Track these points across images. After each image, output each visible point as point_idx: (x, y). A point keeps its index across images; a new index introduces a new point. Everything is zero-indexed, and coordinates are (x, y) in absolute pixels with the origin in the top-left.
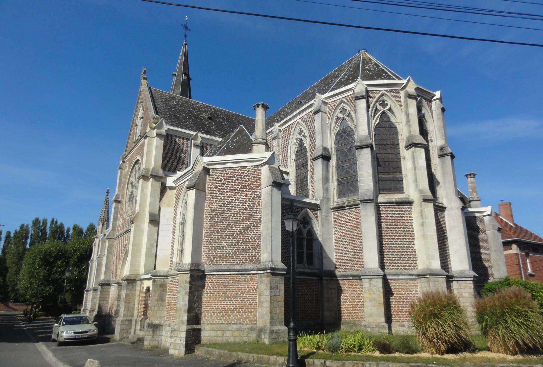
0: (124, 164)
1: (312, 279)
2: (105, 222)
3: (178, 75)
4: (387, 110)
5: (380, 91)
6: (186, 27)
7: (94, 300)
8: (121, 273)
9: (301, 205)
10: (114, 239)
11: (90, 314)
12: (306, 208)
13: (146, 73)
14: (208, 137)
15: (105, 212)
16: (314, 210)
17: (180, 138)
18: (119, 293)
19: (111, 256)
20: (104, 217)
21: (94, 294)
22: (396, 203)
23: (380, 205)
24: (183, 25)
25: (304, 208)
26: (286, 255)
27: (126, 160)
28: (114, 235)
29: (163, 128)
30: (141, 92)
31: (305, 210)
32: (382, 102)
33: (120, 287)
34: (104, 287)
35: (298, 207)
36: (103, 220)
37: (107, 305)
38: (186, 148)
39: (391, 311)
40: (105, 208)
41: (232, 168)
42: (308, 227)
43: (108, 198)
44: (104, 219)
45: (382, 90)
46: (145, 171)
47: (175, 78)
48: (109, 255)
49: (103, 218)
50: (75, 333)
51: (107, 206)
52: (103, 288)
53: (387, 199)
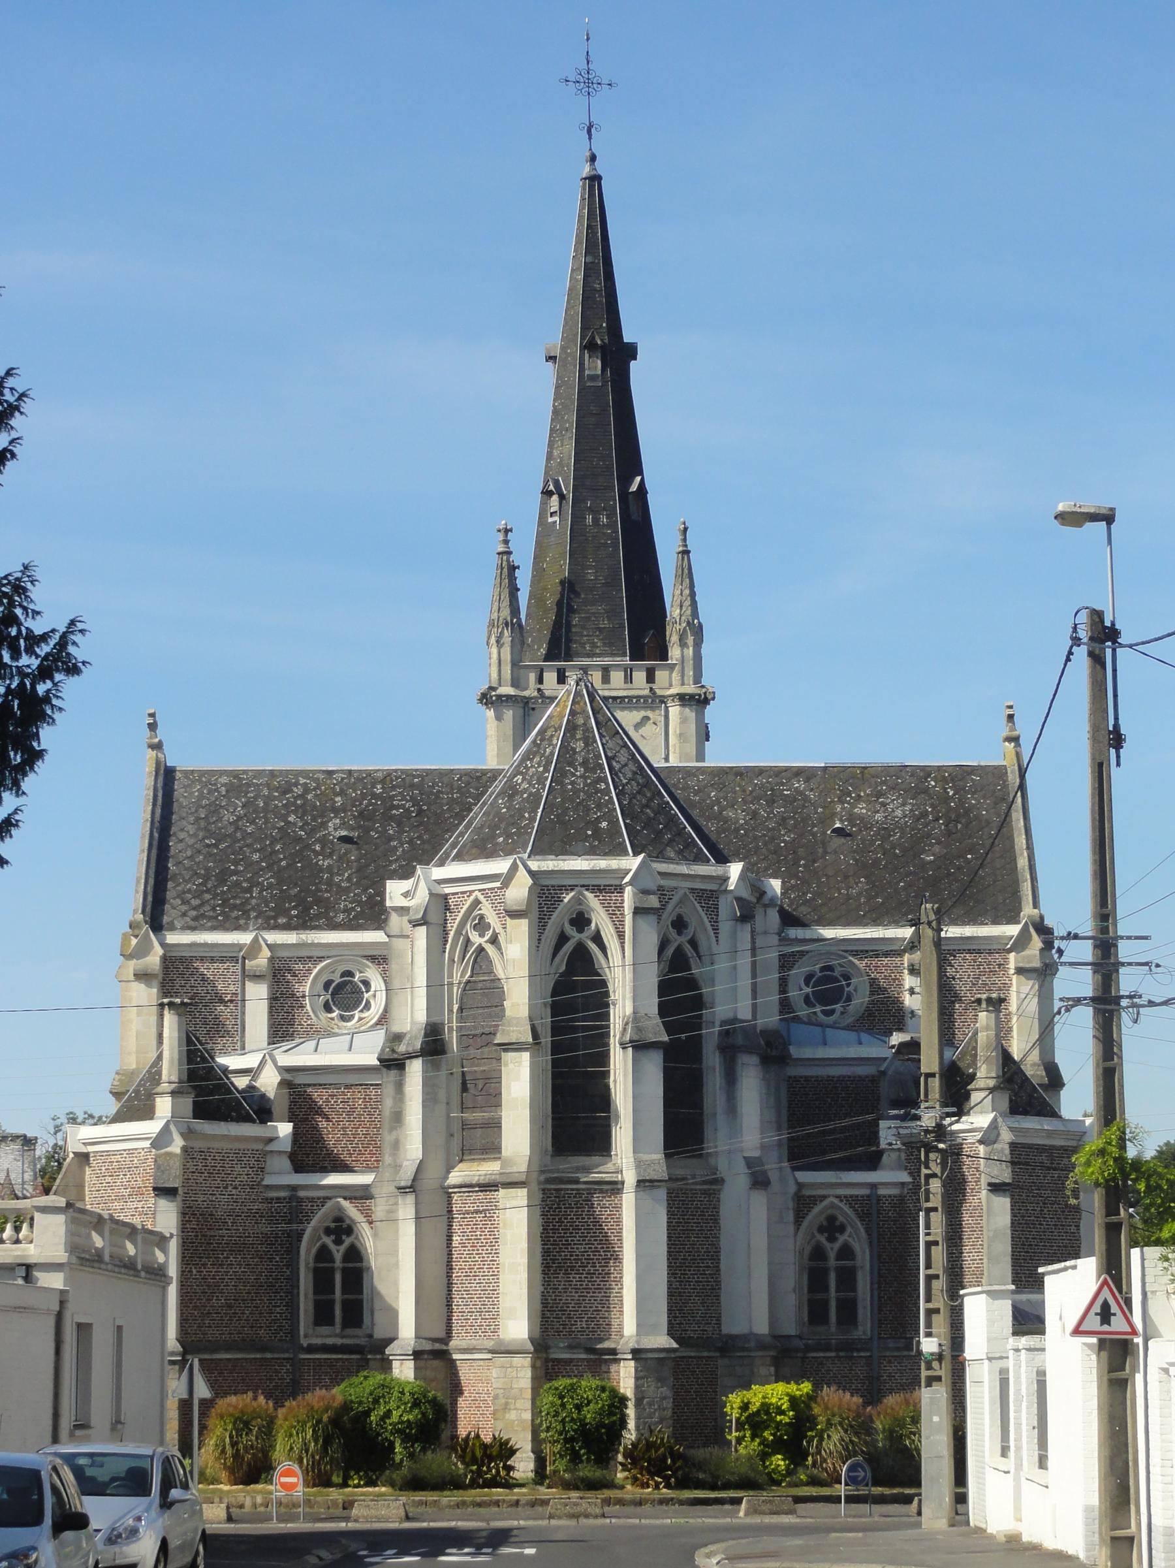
1: (347, 1359)
4: (486, 942)
5: (472, 892)
9: (321, 1194)
12: (336, 1197)
14: (290, 938)
16: (361, 1198)
17: (213, 960)
22: (479, 1185)
23: (450, 1190)
25: (330, 1198)
26: (278, 1309)
29: (152, 953)
31: (329, 1204)
32: (480, 920)
35: (313, 1198)
38: (232, 987)
39: (457, 1428)
41: (125, 1150)
42: (348, 1241)
45: (474, 891)
46: (119, 1080)
53: (466, 1175)
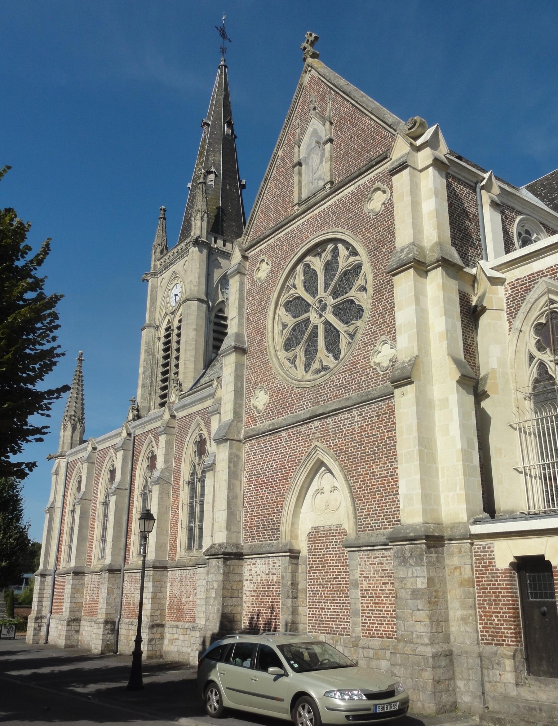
0: (247, 264)
2: (78, 424)
3: (214, 126)
6: (223, 34)
7: (76, 595)
8: (293, 524)
10: (240, 441)
11: (70, 628)
13: (316, 44)
15: (76, 403)
18: (292, 577)
19: (237, 482)
20: (75, 411)
21: (76, 582)
24: (219, 28)
27: (250, 254)
28: (239, 433)
30: (302, 88)
33: (294, 561)
34: (229, 562)
36: (73, 418)
37: (239, 608)
40: (77, 394)
43: (81, 372)
44: (75, 416)
47: (206, 131)
48: (233, 481)
49: (73, 413)
50: (370, 696)
51: (80, 388)
52: (227, 565)
